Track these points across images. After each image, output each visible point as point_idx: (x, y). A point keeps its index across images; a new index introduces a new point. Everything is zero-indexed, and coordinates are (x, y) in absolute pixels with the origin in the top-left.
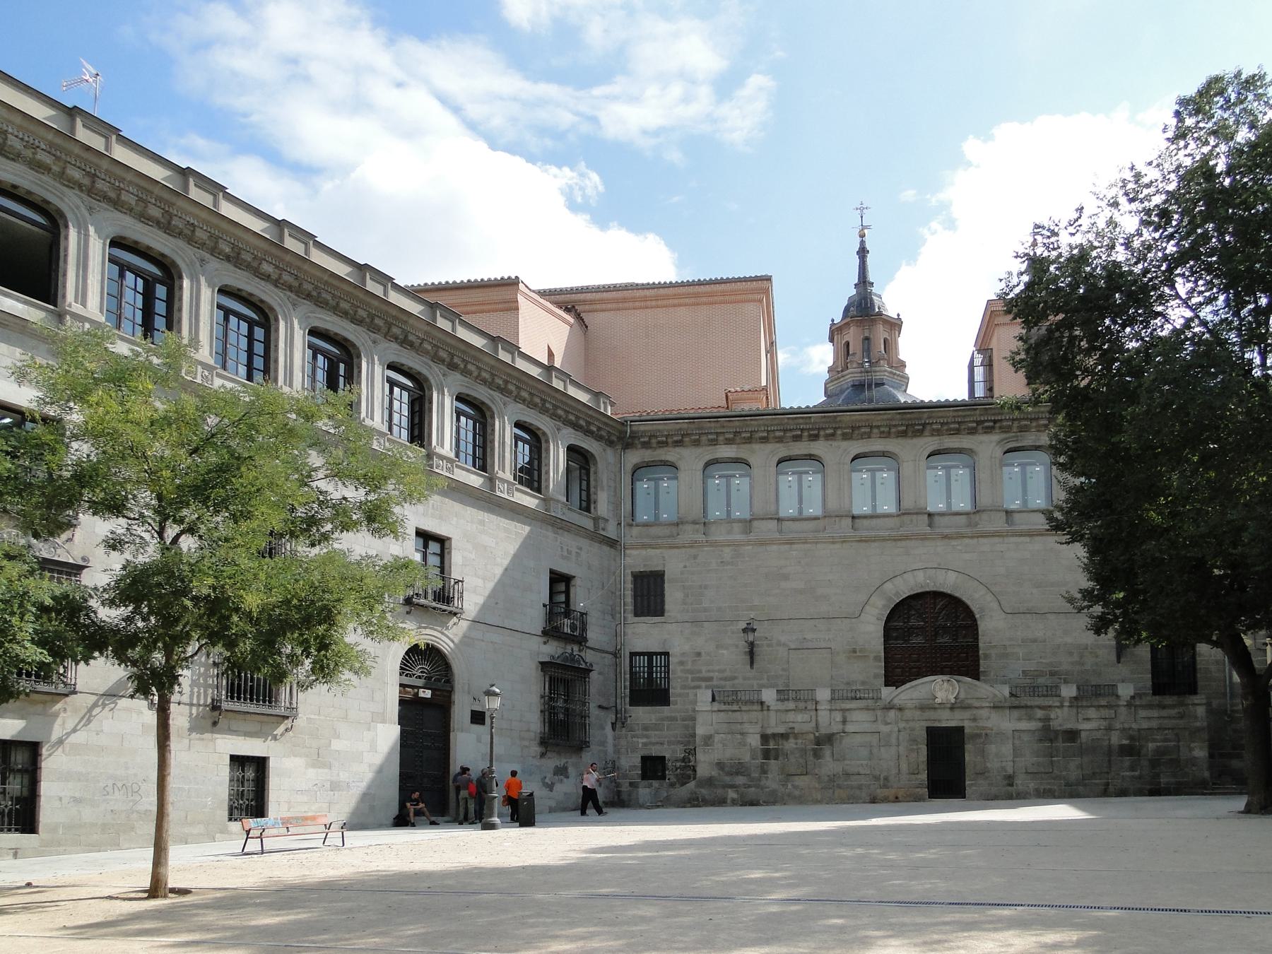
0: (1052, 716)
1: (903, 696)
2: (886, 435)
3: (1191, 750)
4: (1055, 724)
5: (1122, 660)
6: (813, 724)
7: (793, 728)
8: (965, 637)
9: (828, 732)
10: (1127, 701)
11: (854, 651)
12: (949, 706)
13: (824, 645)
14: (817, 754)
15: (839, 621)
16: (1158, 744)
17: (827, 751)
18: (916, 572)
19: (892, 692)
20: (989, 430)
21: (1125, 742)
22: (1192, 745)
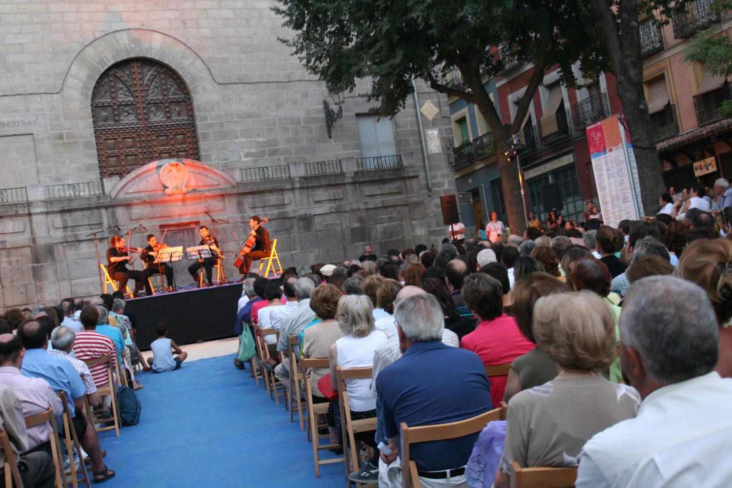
0: (286, 202)
1: (131, 189)
3: (413, 228)
4: (289, 209)
5: (333, 134)
6: (27, 235)
7: (5, 242)
8: (179, 114)
9: (48, 241)
10: (352, 178)
11: (61, 137)
12: (180, 197)
13: (22, 129)
14: (37, 274)
15: (38, 98)
16: (385, 225)
17: (48, 270)
18: (117, 35)
19: (116, 185)
21: (356, 225)
22: (414, 223)
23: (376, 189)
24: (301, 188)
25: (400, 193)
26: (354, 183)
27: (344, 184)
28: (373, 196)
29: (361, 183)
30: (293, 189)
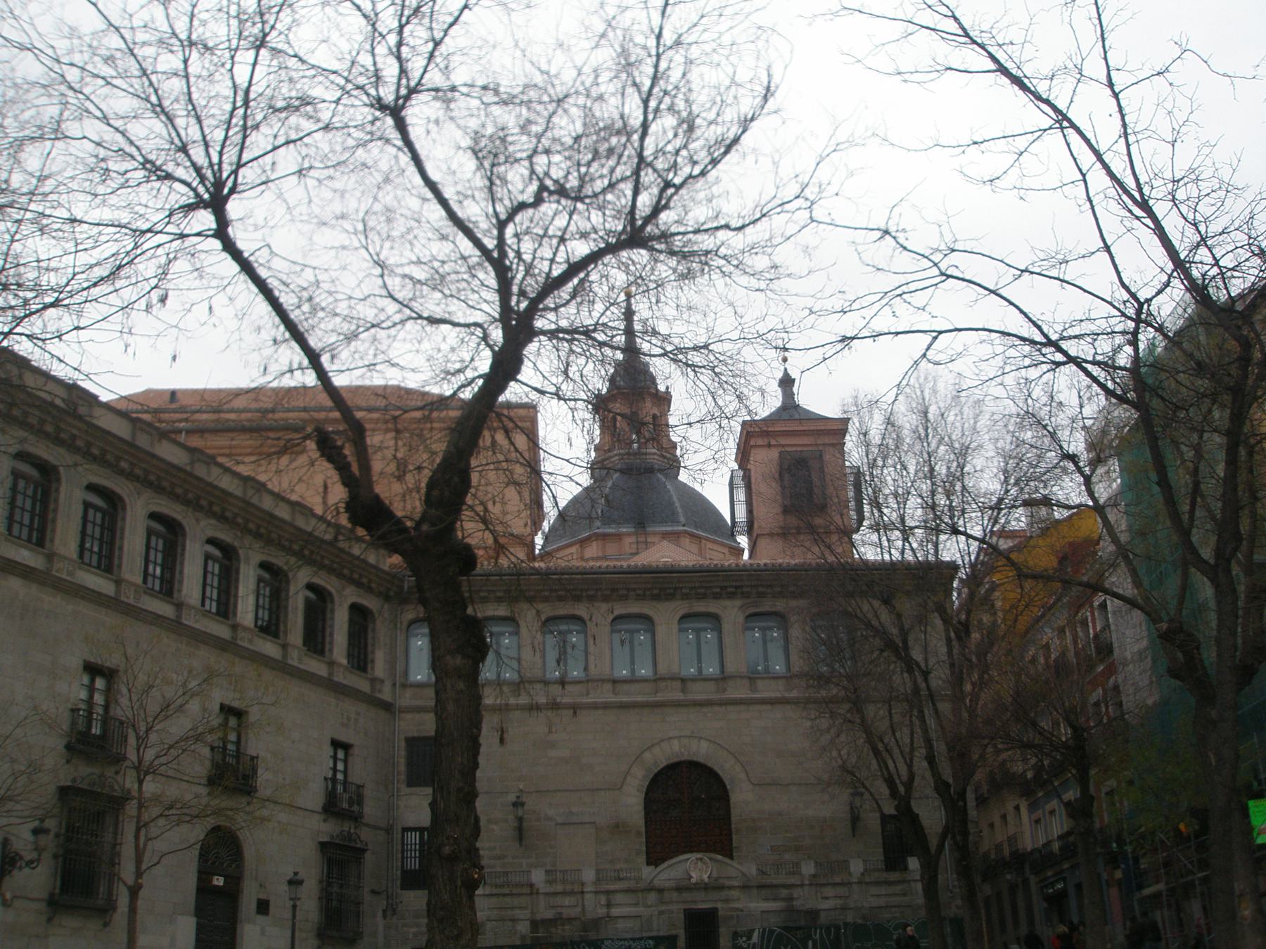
1: (663, 876)
2: (641, 597)
6: (579, 909)
20: (731, 596)
23: (882, 890)
24: (811, 885)
25: (905, 895)
26: (860, 883)
27: (850, 884)
28: (879, 896)
29: (867, 883)
30: (802, 885)
